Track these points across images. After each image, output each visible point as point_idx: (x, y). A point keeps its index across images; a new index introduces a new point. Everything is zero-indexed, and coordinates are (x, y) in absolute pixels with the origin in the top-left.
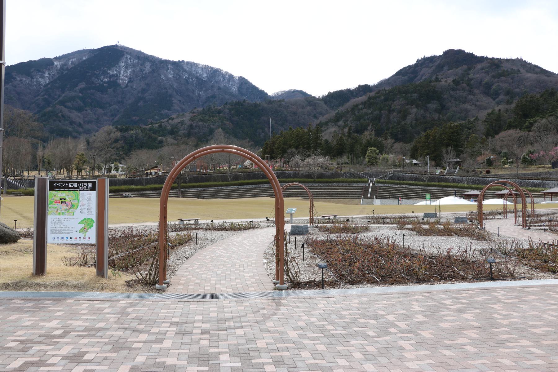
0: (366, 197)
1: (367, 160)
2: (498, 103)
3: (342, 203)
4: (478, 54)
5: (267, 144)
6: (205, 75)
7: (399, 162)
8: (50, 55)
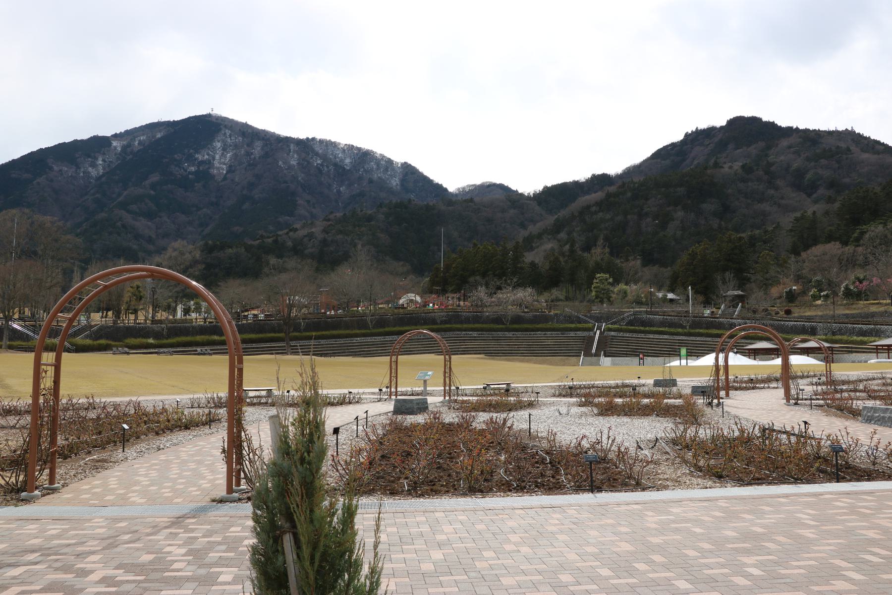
0: (588, 354)
1: (594, 293)
2: (816, 202)
3: (551, 364)
4: (783, 123)
5: (438, 269)
6: (348, 161)
7: (646, 297)
8: (107, 131)
